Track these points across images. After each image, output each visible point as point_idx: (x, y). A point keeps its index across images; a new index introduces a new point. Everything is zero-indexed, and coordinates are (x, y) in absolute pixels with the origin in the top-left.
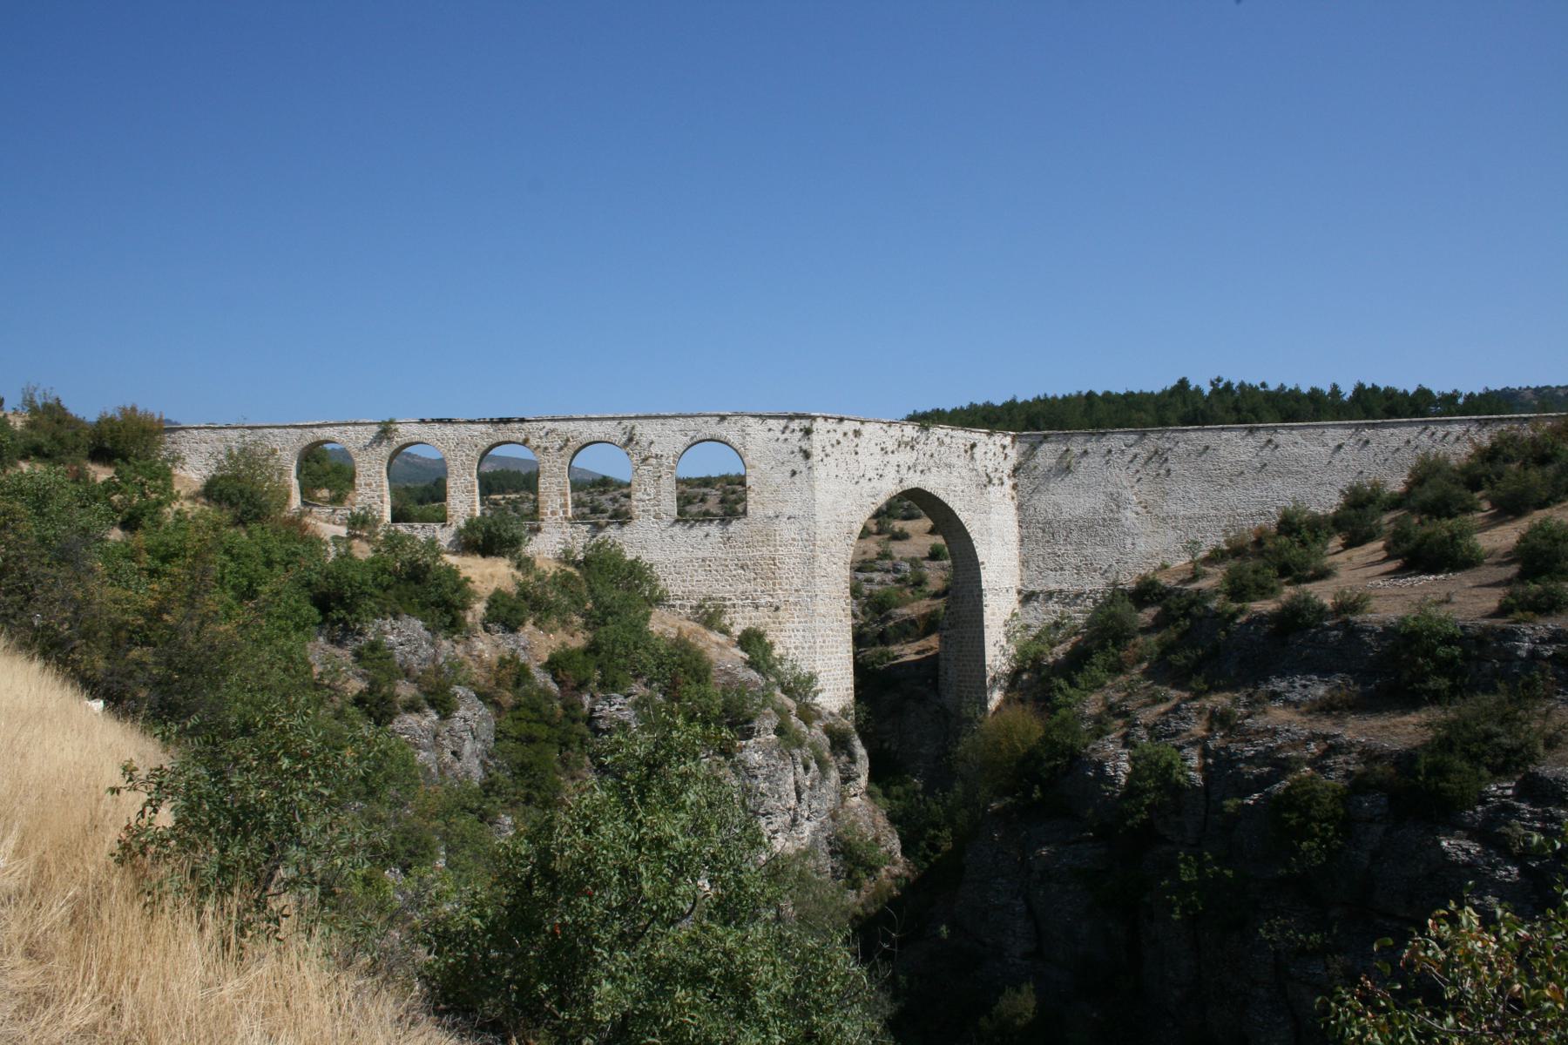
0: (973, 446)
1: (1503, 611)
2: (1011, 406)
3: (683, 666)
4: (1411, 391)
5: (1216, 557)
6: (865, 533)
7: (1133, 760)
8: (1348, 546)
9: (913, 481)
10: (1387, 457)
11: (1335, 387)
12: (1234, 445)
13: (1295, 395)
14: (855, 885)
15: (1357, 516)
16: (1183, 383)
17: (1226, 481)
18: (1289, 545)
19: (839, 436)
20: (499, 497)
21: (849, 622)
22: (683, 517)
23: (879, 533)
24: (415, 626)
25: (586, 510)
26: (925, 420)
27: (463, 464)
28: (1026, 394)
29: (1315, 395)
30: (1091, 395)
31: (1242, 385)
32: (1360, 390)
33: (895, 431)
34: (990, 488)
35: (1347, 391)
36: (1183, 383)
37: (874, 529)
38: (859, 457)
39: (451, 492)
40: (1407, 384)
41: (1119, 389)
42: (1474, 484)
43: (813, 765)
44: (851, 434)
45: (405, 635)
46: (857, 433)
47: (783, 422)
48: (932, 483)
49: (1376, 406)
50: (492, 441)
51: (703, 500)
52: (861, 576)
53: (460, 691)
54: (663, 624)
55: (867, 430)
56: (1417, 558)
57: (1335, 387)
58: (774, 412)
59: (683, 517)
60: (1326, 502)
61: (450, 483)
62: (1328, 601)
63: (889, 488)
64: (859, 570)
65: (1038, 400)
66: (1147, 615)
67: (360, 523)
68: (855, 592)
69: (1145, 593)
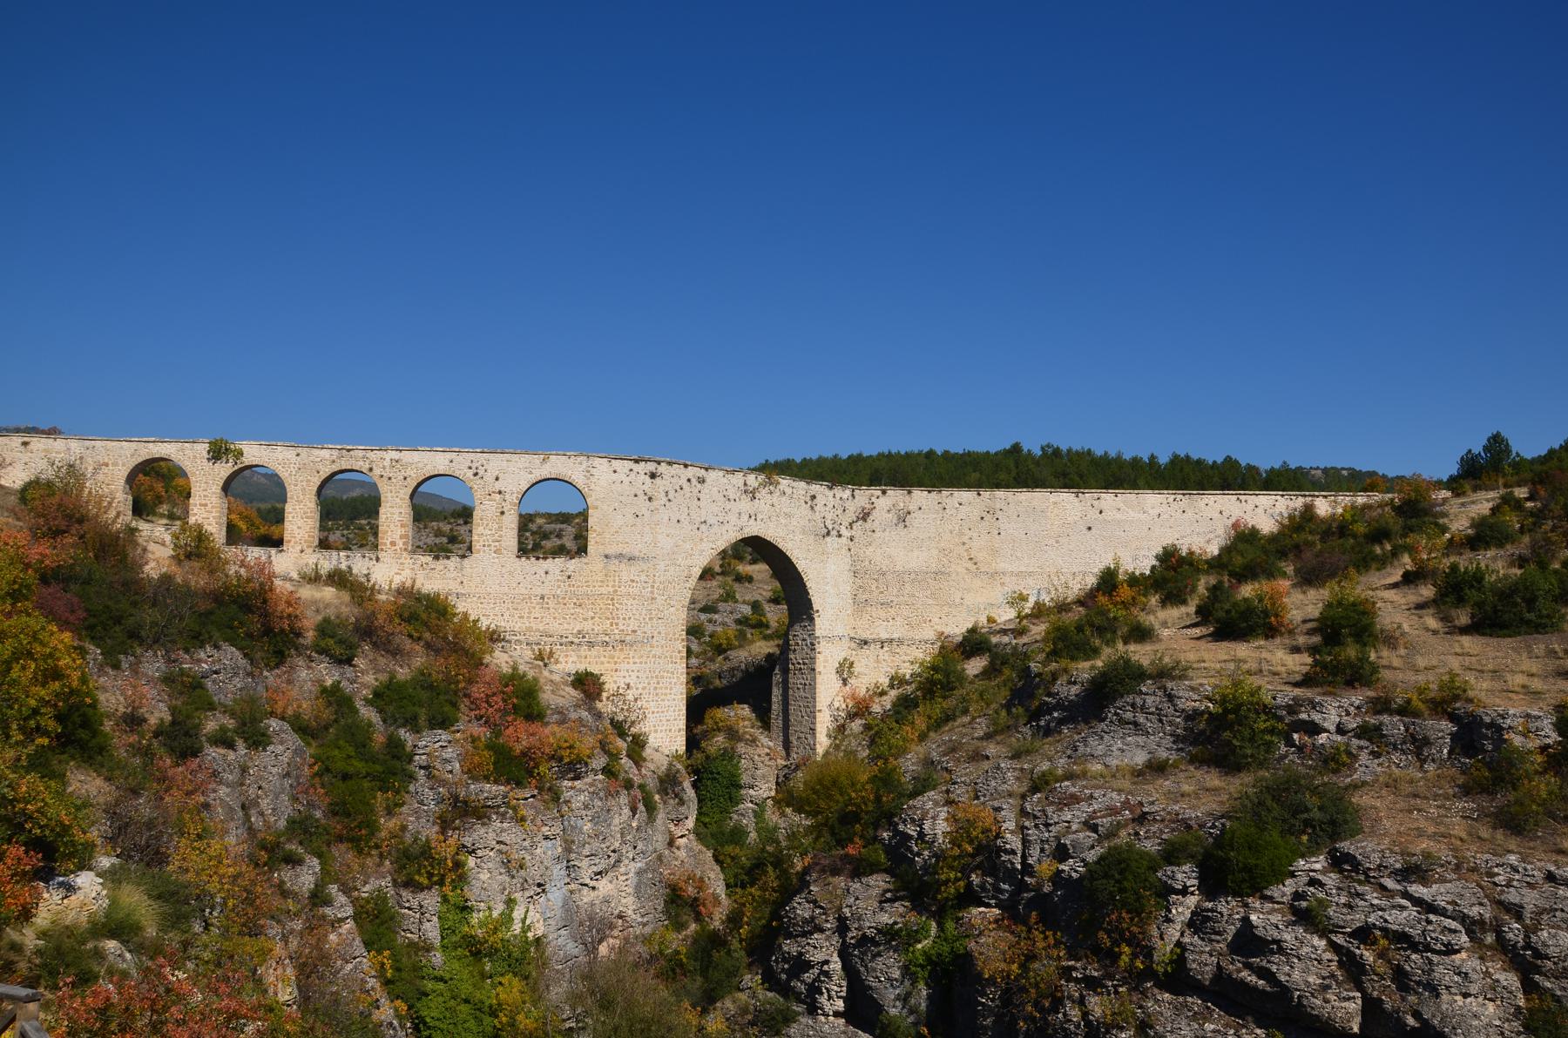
0: (814, 497)
1: (1307, 681)
2: (856, 460)
3: (522, 698)
4: (1219, 460)
5: (1039, 612)
6: (706, 574)
7: (953, 819)
8: (1164, 603)
9: (753, 529)
10: (1201, 523)
11: (1153, 457)
12: (1062, 505)
13: (1118, 460)
14: (680, 927)
15: (1173, 574)
16: (1016, 448)
17: (1052, 541)
18: (1108, 604)
19: (683, 482)
20: (364, 522)
21: (681, 667)
22: (523, 551)
23: (723, 573)
24: (231, 655)
25: (445, 540)
26: (774, 469)
27: (303, 489)
28: (870, 450)
29: (1136, 462)
30: (931, 454)
31: (1069, 451)
32: (1175, 460)
33: (738, 479)
34: (828, 539)
35: (1163, 459)
36: (1016, 448)
37: (717, 569)
38: (701, 503)
39: (288, 517)
40: (1212, 454)
41: (957, 448)
42: (1282, 554)
43: (641, 807)
44: (694, 481)
45: (223, 667)
46: (702, 481)
47: (631, 464)
48: (771, 533)
49: (1333, 481)
50: (335, 468)
51: (559, 536)
52: (703, 617)
53: (274, 724)
54: (500, 660)
55: (712, 476)
56: (1229, 623)
57: (1153, 457)
58: (12, 425)
59: (523, 551)
60: (1142, 562)
61: (288, 508)
62: (1145, 662)
63: (727, 537)
64: (704, 610)
65: (881, 455)
66: (974, 666)
67: (195, 548)
68: (694, 631)
69: (973, 643)
